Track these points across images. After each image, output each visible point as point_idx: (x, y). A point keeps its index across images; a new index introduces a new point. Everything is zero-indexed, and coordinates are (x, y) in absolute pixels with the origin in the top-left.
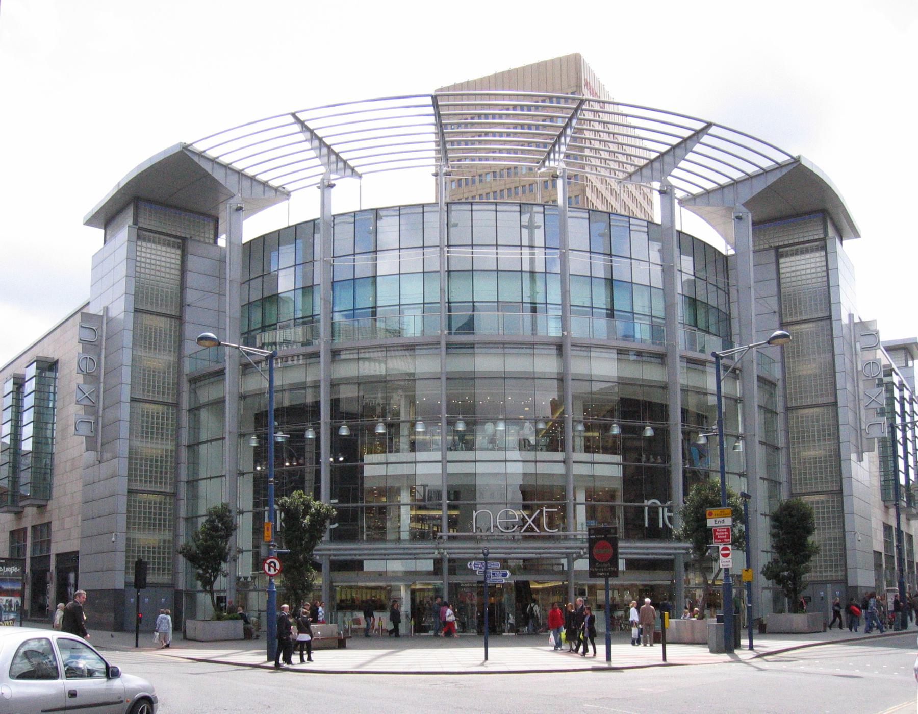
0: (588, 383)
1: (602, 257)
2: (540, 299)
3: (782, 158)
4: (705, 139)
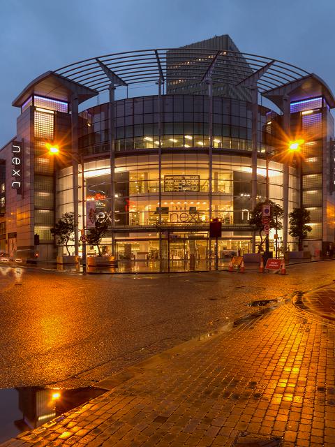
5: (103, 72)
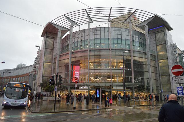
0: (115, 56)
1: (75, 44)
2: (134, 40)
3: (153, 15)
4: (136, 13)
5: (68, 21)
